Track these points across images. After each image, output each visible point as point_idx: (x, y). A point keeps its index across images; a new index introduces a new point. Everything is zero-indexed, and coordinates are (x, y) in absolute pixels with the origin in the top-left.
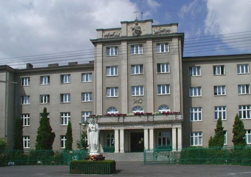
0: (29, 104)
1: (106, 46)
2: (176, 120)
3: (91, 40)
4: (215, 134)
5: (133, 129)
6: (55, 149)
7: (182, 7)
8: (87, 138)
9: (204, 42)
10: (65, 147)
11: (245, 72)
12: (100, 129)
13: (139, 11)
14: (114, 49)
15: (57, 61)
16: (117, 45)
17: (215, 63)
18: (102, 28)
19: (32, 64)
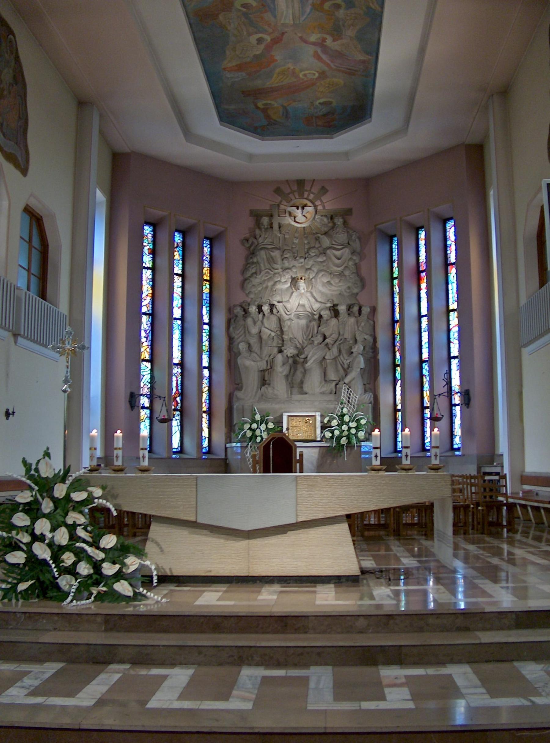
0: (169, 600)
1: (382, 705)
2: (29, 270)
3: (24, 171)
4: (12, 522)
5: (447, 592)
6: (316, 338)
7: (88, 566)
8: (94, 558)
9: (544, 294)
10: (131, 607)
11: (329, 696)
12: (450, 530)
13: (39, 249)
14: (432, 580)
15: (197, 497)
16: (187, 705)
17: (497, 378)
18: (264, 142)
19: (46, 698)
